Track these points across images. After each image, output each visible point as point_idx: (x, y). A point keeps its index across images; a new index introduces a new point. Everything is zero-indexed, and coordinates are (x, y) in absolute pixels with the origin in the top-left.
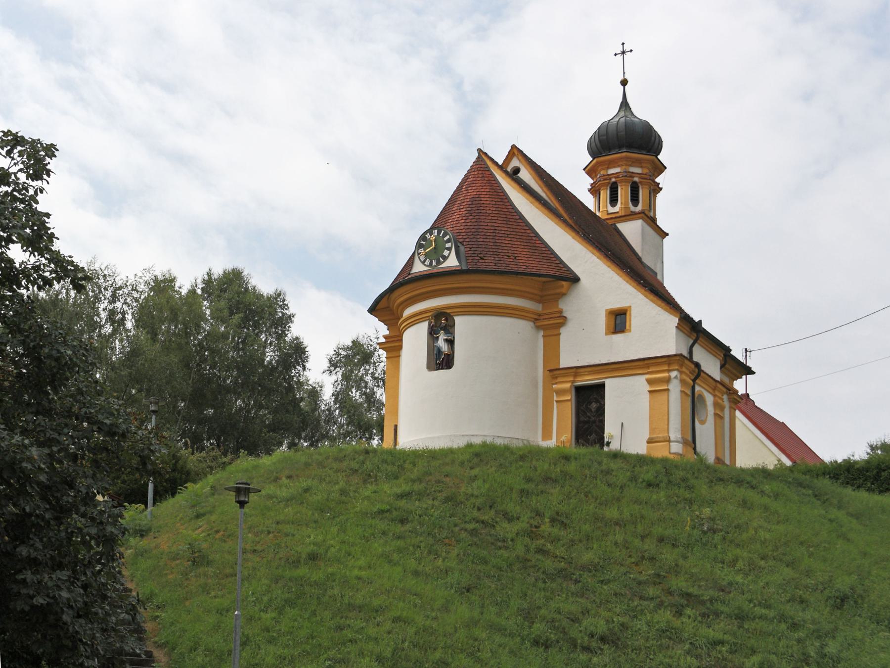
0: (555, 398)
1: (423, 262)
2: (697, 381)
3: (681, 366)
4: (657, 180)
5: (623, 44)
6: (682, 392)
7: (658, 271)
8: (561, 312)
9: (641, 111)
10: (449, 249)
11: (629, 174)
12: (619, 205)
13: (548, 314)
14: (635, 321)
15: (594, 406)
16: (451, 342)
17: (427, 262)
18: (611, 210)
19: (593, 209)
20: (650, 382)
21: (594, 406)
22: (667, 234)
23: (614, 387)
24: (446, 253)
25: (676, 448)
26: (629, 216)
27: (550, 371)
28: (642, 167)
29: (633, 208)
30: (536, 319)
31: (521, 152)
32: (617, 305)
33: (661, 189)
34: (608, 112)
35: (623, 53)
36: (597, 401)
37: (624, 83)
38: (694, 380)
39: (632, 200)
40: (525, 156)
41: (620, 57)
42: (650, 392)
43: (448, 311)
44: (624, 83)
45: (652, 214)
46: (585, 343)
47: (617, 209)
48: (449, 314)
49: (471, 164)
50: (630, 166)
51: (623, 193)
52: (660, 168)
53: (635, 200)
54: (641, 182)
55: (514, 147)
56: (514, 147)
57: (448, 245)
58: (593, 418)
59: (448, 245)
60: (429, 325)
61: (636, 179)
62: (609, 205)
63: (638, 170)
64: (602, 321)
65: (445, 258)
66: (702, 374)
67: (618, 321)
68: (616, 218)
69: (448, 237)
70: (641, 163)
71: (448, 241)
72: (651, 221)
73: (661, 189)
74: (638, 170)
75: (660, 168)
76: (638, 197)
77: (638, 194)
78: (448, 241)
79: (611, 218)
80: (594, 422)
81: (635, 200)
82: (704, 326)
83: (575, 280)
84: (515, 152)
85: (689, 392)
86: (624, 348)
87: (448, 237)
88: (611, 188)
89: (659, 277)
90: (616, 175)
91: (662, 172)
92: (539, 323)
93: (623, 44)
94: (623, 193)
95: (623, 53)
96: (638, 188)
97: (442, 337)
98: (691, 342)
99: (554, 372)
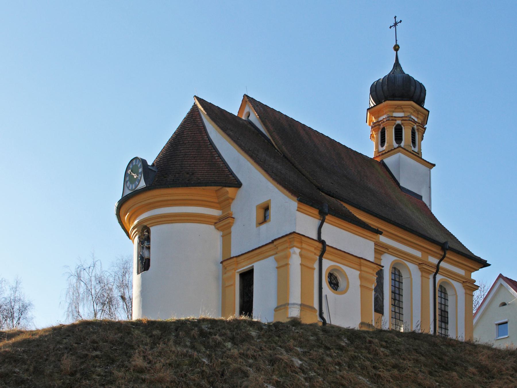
2: (325, 255)
3: (301, 243)
5: (395, 17)
6: (466, 293)
7: (423, 193)
11: (391, 118)
12: (386, 145)
19: (368, 149)
28: (404, 112)
32: (262, 200)
34: (384, 71)
37: (396, 48)
39: (396, 139)
44: (396, 48)
45: (416, 150)
47: (384, 148)
50: (393, 112)
51: (390, 134)
54: (402, 124)
55: (246, 96)
62: (380, 146)
66: (327, 248)
68: (383, 154)
70: (402, 108)
72: (417, 156)
83: (238, 184)
84: (248, 100)
89: (424, 200)
93: (395, 17)
95: (396, 24)
96: (401, 129)
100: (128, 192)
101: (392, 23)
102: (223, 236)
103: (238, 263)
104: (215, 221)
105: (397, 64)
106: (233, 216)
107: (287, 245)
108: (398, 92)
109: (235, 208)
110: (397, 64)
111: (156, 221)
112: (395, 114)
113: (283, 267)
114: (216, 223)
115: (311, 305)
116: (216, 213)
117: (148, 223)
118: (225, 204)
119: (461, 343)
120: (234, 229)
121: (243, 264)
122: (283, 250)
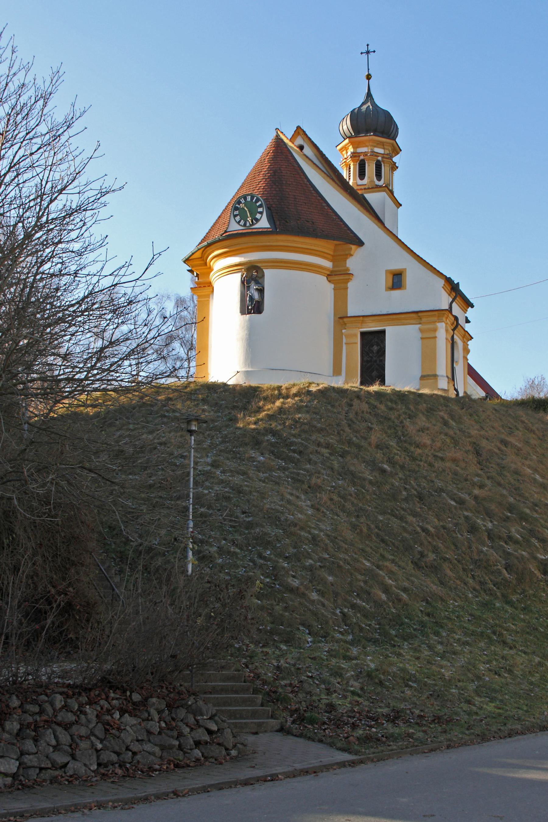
0: (344, 340)
1: (239, 223)
4: (394, 159)
8: (348, 269)
9: (382, 102)
10: (261, 213)
13: (339, 271)
14: (409, 279)
15: (375, 348)
16: (261, 291)
17: (242, 223)
18: (360, 182)
20: (421, 331)
21: (375, 348)
22: (401, 205)
23: (393, 335)
24: (258, 216)
25: (443, 383)
26: (377, 188)
27: (340, 318)
28: (384, 149)
29: (377, 183)
30: (330, 275)
31: (304, 132)
32: (396, 266)
33: (397, 167)
34: (356, 101)
35: (368, 52)
36: (378, 345)
37: (369, 77)
38: (453, 330)
40: (306, 135)
41: (365, 56)
42: (422, 338)
43: (259, 265)
44: (369, 77)
46: (368, 297)
47: (365, 181)
48: (257, 267)
49: (327, 156)
50: (375, 147)
51: (370, 169)
52: (397, 150)
53: (379, 175)
55: (298, 128)
56: (298, 128)
57: (260, 210)
58: (374, 359)
59: (260, 210)
60: (242, 276)
61: (380, 158)
62: (358, 178)
63: (381, 151)
64: (382, 280)
65: (257, 220)
67: (397, 280)
68: (365, 189)
69: (260, 203)
71: (261, 206)
73: (397, 167)
74: (381, 151)
75: (397, 150)
76: (381, 173)
77: (381, 171)
78: (261, 206)
79: (361, 189)
80: (376, 361)
81: (379, 175)
82: (461, 288)
84: (299, 131)
85: (450, 339)
86: (398, 301)
87: (260, 203)
88: (360, 164)
90: (365, 154)
91: (398, 153)
92: (330, 278)
93: (368, 45)
94: (370, 169)
95: (368, 52)
97: (254, 286)
98: (451, 300)
99: (342, 319)
100: (235, 227)
101: (365, 50)
102: (334, 289)
103: (363, 322)
104: (328, 273)
105: (369, 95)
106: (350, 272)
107: (436, 319)
108: (373, 124)
109: (351, 263)
110: (369, 95)
111: (275, 264)
112: (377, 150)
113: (428, 339)
114: (329, 275)
115: (434, 373)
116: (328, 264)
117: (264, 265)
118: (339, 259)
119: (474, 401)
120: (351, 285)
121: (371, 325)
122: (430, 323)
